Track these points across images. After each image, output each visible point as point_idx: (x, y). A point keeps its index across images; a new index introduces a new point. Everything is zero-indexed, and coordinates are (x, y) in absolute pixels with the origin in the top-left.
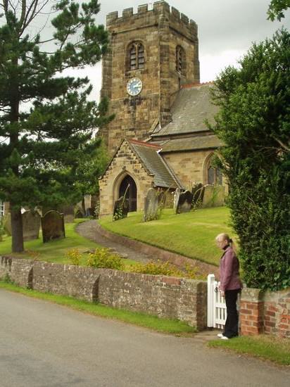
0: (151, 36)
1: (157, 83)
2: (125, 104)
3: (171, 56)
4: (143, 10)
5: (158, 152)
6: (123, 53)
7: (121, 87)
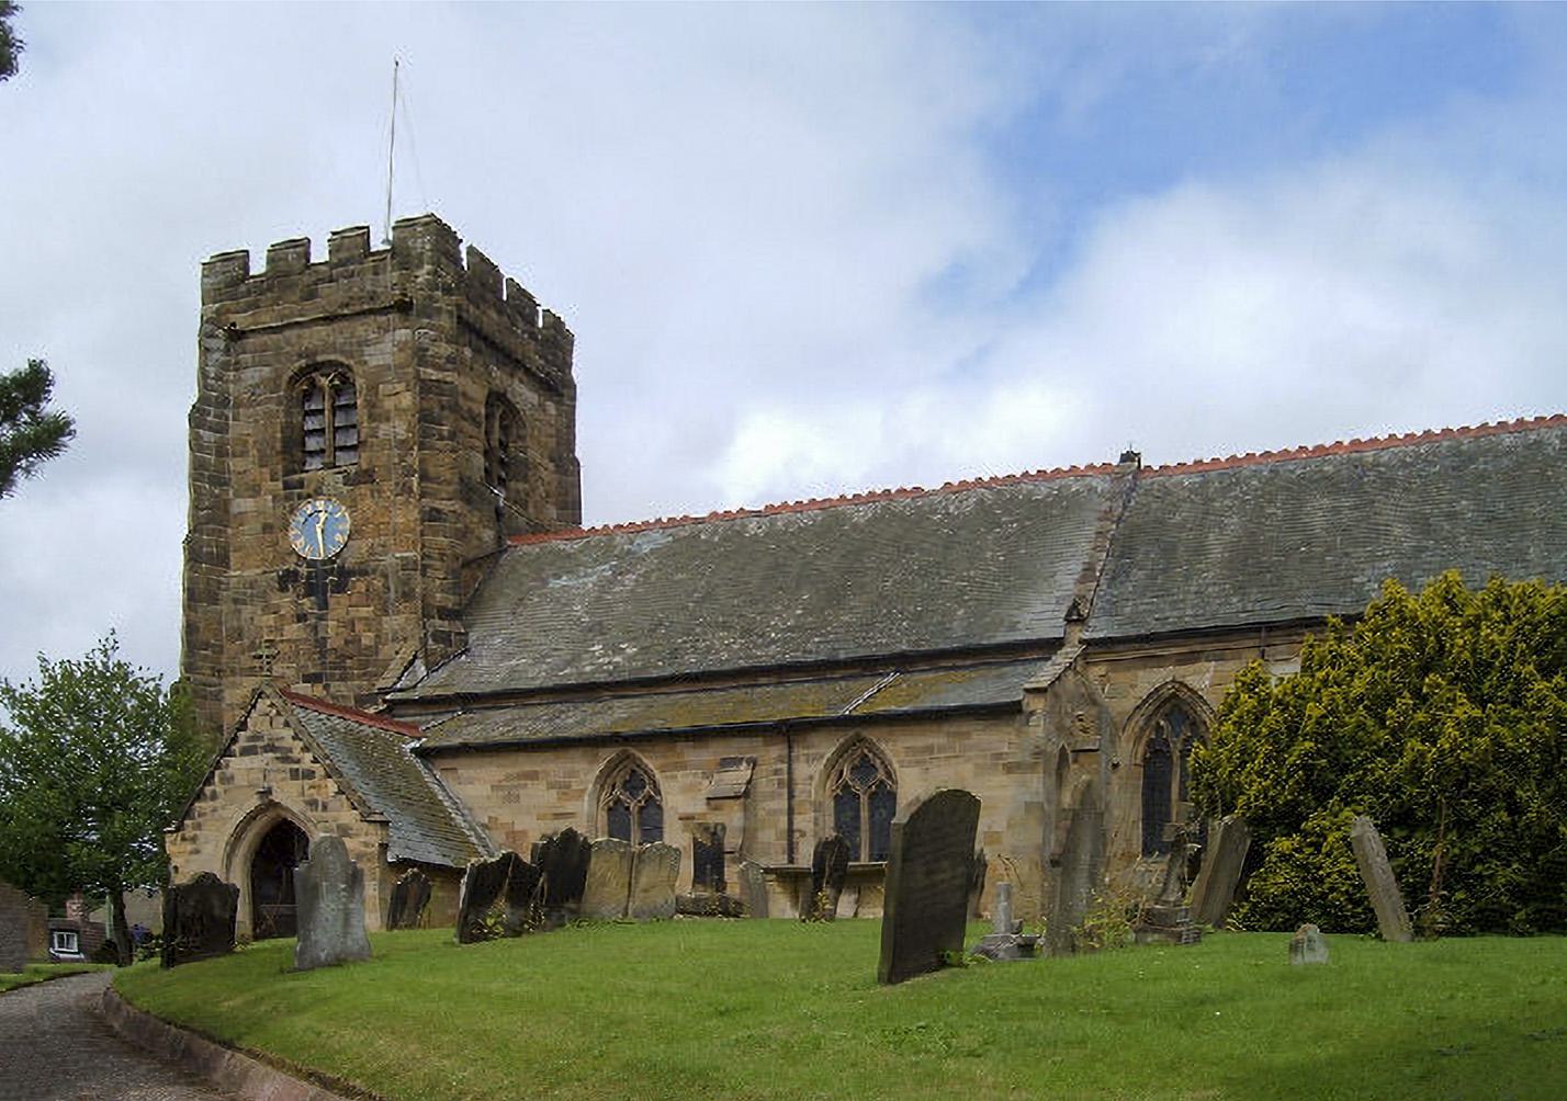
0: (382, 347)
1: (406, 516)
2: (283, 589)
3: (467, 426)
4: (351, 244)
5: (408, 747)
6: (273, 407)
7: (267, 528)
